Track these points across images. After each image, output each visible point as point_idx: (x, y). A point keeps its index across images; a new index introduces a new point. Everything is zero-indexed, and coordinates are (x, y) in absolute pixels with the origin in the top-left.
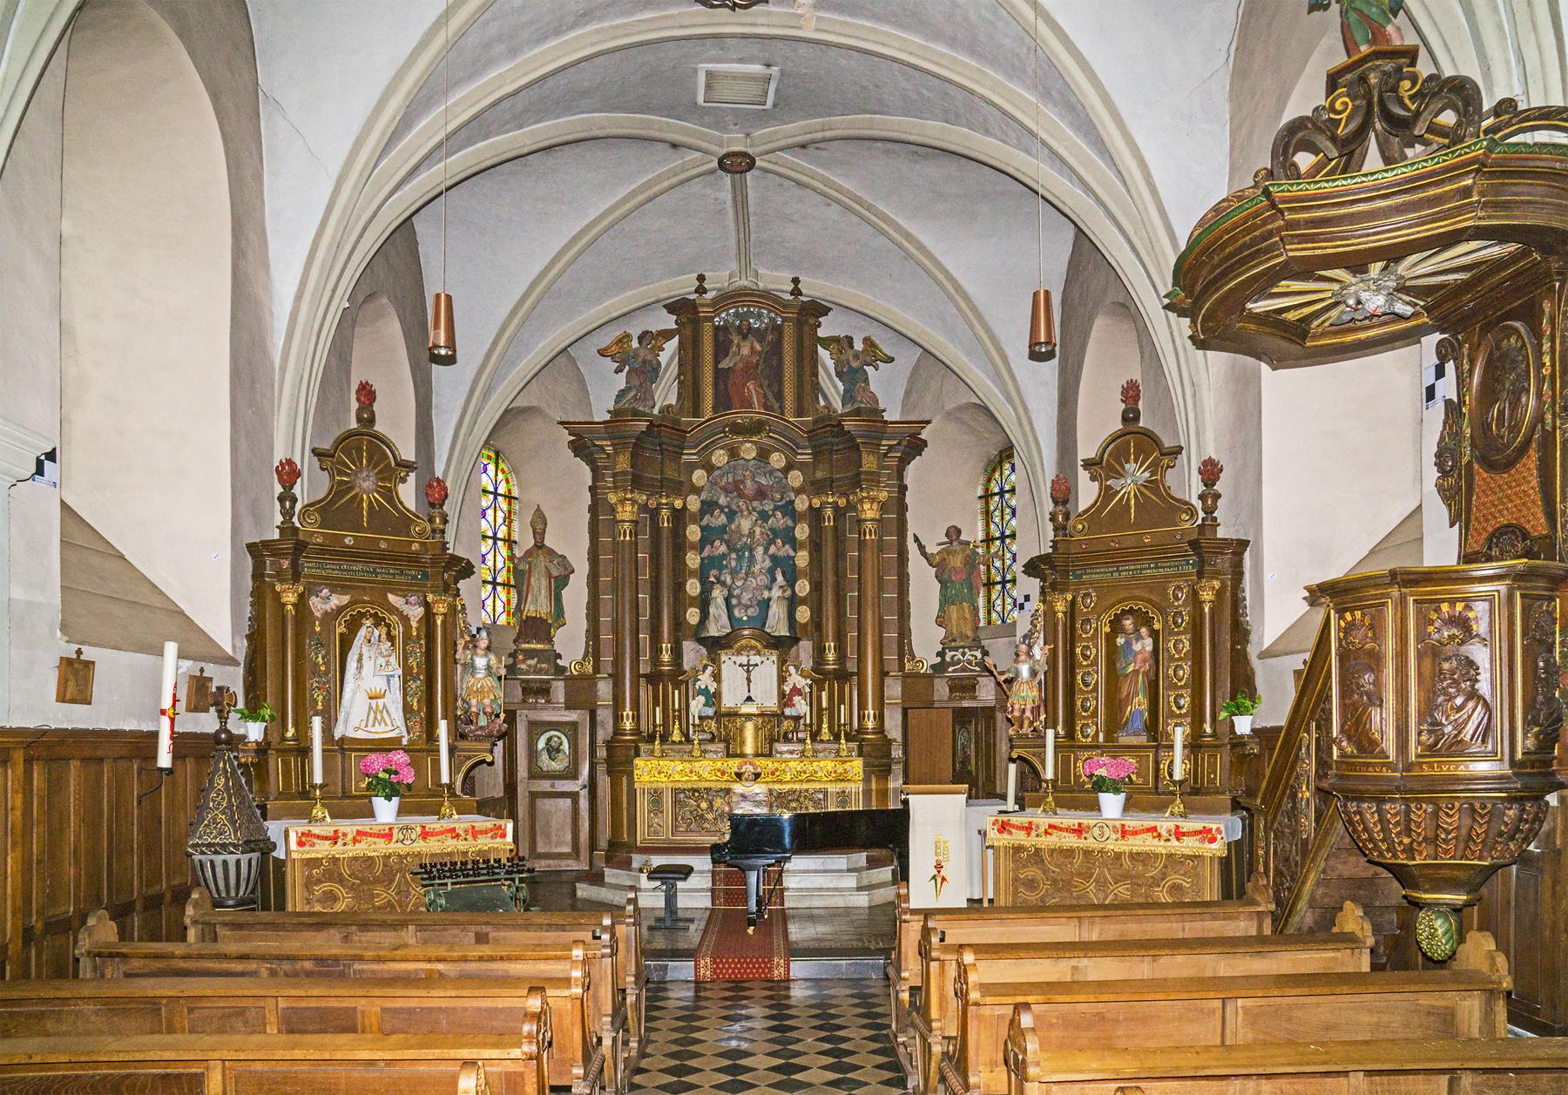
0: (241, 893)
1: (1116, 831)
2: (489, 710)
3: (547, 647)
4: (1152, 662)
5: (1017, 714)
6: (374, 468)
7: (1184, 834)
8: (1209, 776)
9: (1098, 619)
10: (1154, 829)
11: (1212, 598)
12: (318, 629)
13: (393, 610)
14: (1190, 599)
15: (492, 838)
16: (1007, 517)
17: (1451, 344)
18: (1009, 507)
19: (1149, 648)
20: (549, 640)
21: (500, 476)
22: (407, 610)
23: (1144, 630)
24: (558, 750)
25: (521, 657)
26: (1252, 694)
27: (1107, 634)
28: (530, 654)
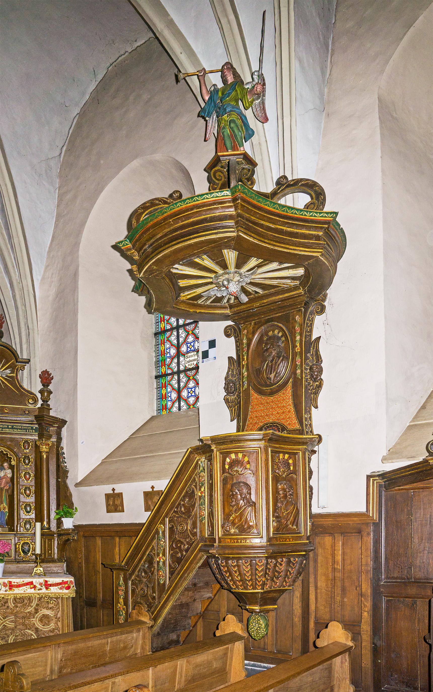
4: (11, 484)
7: (51, 585)
8: (48, 552)
10: (31, 583)
11: (48, 450)
14: (34, 449)
17: (235, 330)
19: (10, 475)
26: (71, 505)
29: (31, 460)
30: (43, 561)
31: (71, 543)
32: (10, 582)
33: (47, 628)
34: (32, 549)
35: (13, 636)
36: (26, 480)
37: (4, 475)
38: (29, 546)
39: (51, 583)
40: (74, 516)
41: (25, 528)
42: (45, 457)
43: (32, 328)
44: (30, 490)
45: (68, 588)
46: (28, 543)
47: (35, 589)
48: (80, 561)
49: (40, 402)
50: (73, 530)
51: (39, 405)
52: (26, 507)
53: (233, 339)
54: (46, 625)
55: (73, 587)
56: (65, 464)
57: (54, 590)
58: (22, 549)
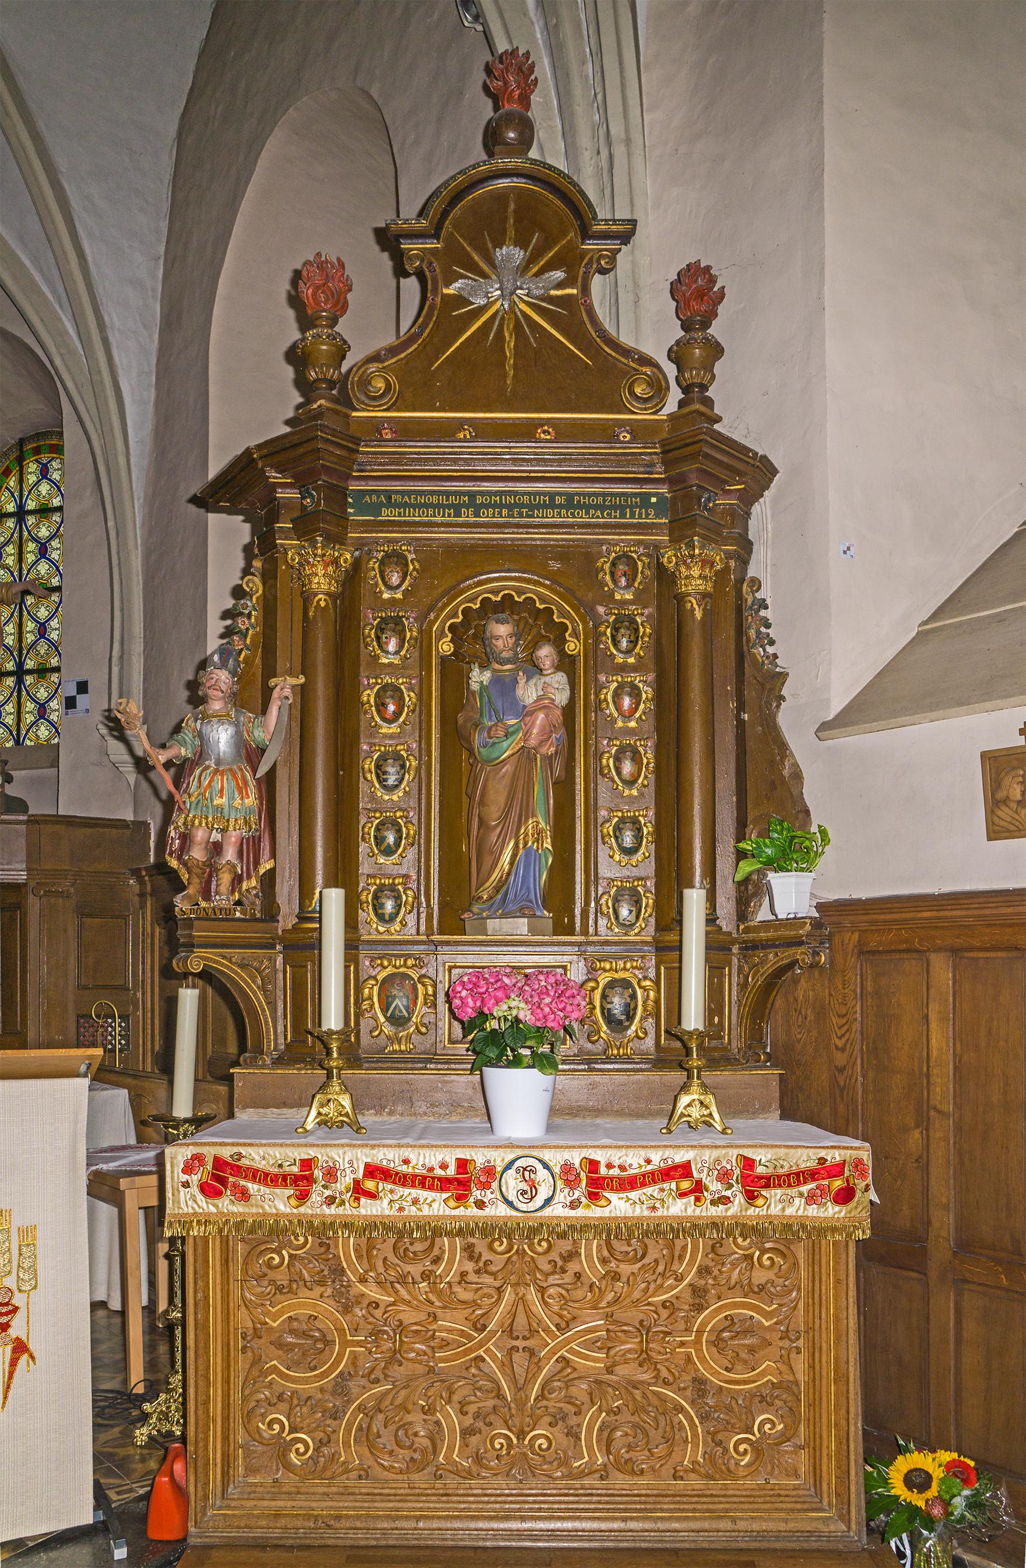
1: (571, 1183)
5: (198, 854)
7: (768, 1182)
9: (422, 618)
10: (685, 1170)
11: (710, 587)
16: (30, 558)
18: (35, 540)
19: (562, 698)
23: (546, 653)
27: (443, 660)
29: (641, 630)
31: (796, 981)
32: (593, 1165)
33: (745, 1382)
34: (645, 1010)
35: (600, 1410)
36: (624, 716)
37: (539, 699)
38: (634, 996)
40: (821, 863)
41: (617, 918)
42: (698, 614)
43: (623, 135)
44: (636, 758)
45: (845, 1196)
46: (626, 984)
47: (697, 1199)
48: (840, 1059)
49: (675, 395)
50: (817, 924)
51: (671, 405)
52: (620, 830)
53: (751, 572)
54: (739, 1367)
55: (867, 1188)
56: (770, 650)
58: (602, 1008)
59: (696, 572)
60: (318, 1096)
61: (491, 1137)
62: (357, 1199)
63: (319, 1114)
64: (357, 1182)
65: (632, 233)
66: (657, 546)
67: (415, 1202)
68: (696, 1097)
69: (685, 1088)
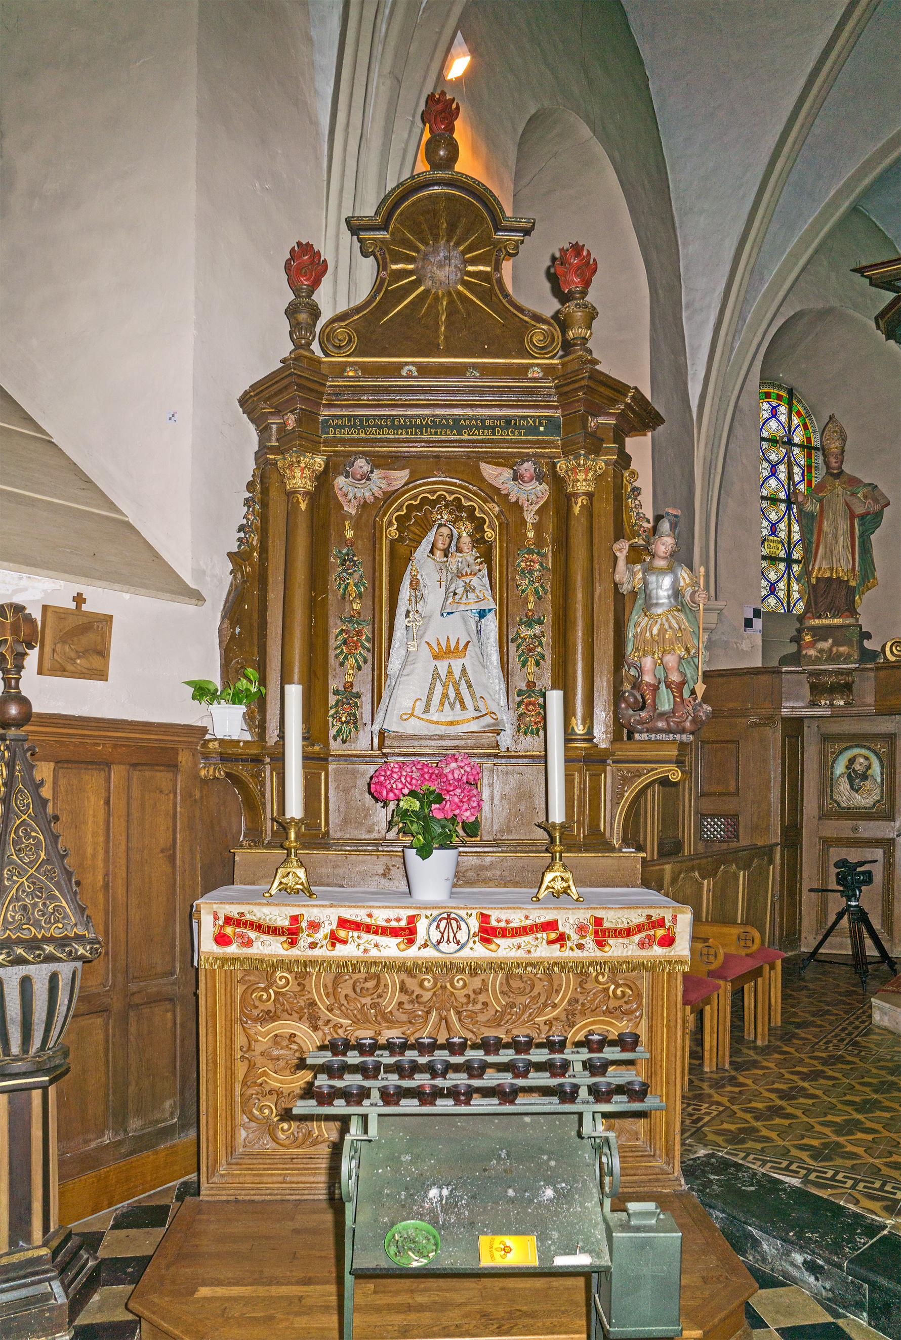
0: (36, 1043)
2: (675, 677)
3: (849, 621)
6: (457, 244)
10: (551, 926)
12: (349, 534)
13: (493, 493)
15: (642, 945)
20: (852, 611)
21: (796, 421)
22: (515, 492)
24: (864, 777)
25: (808, 638)
28: (821, 633)
30: (571, 846)
39: (612, 926)
47: (562, 946)
57: (618, 949)
59: (581, 476)
60: (280, 870)
61: (410, 900)
62: (333, 945)
63: (281, 883)
64: (332, 932)
65: (533, 228)
66: (551, 457)
67: (376, 945)
68: (558, 874)
69: (549, 868)
